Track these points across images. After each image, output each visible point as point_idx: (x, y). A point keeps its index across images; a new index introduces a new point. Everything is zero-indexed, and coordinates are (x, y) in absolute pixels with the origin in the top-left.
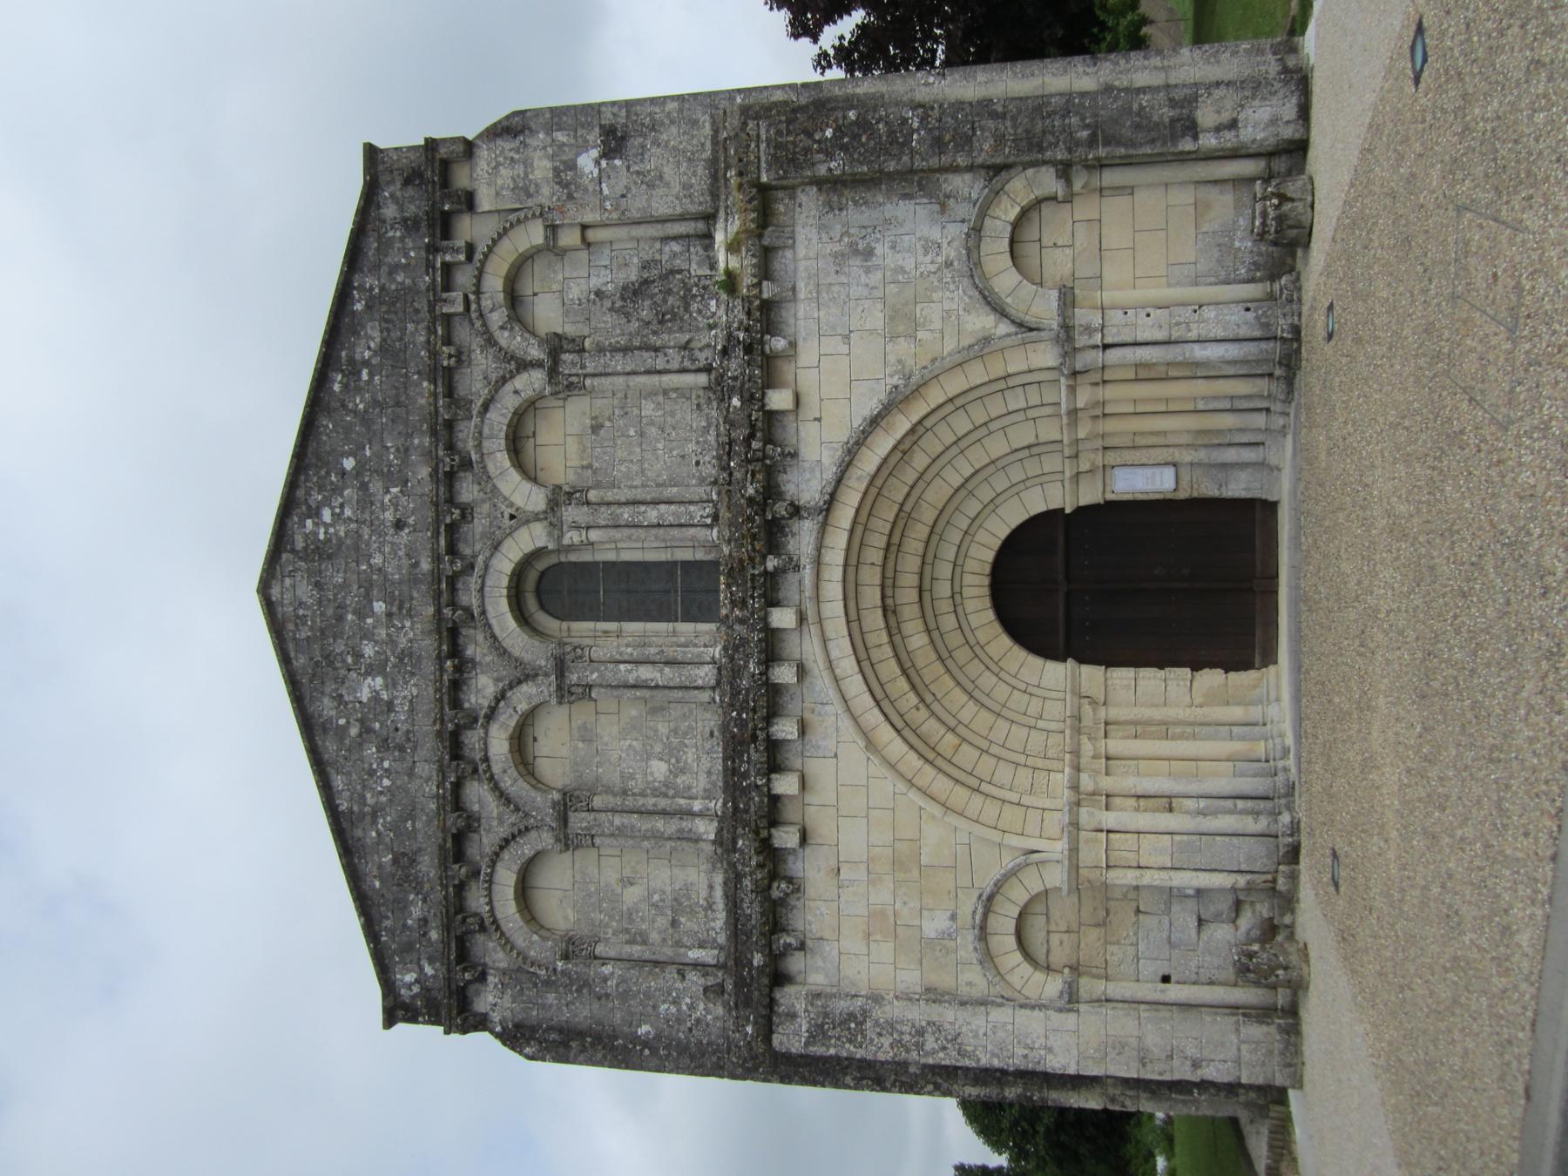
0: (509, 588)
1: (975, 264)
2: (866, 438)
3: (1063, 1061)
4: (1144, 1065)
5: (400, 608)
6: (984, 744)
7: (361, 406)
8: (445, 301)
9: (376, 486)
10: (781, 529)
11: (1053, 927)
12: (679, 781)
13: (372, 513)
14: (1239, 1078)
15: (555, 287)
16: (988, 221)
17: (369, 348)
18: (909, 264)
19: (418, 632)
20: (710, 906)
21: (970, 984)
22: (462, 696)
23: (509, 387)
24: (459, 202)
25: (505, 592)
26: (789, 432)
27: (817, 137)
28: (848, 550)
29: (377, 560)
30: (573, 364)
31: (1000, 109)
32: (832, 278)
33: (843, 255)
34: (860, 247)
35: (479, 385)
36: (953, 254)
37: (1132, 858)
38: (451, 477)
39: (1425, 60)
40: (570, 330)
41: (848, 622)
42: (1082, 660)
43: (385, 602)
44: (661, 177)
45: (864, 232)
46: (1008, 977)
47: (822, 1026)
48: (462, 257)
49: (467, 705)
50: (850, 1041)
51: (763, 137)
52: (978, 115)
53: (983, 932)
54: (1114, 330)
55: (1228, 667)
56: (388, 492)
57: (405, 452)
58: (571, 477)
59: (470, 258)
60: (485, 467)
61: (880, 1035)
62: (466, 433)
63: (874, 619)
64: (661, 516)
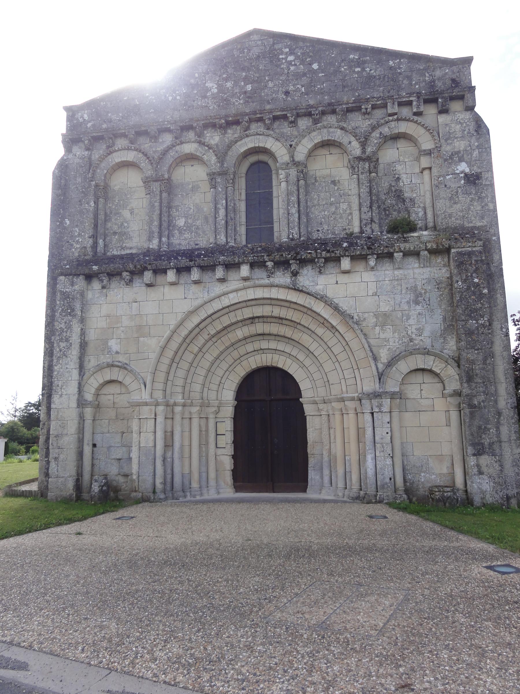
0: (259, 147)
1: (411, 352)
2: (328, 305)
3: (56, 402)
4: (55, 437)
5: (249, 97)
6: (195, 365)
7: (343, 69)
8: (393, 104)
9: (305, 80)
10: (286, 269)
11: (116, 396)
12: (176, 231)
13: (292, 80)
14: (51, 477)
15: (401, 158)
16: (432, 358)
17: (371, 70)
18: (411, 322)
19: (238, 107)
20: (123, 248)
21: (89, 361)
22: (210, 129)
23: (353, 139)
24: (443, 106)
25: (257, 145)
26: (331, 268)
27: (474, 275)
28: (278, 300)
29: (270, 84)
30: (364, 168)
31: (488, 362)
32: (404, 286)
33: (416, 291)
34: (420, 298)
35: (353, 125)
36: (416, 342)
37: (144, 429)
38: (310, 114)
39: (504, 573)
40: (381, 167)
41: (246, 301)
42: (237, 408)
43: (251, 90)
44: (455, 203)
45: (427, 300)
46: (92, 377)
47: (69, 298)
48: (415, 110)
49: (205, 132)
50: (62, 310)
51: (474, 249)
52: (485, 352)
53: (111, 366)
54: (380, 418)
55: (235, 473)
56: (302, 86)
57: (322, 92)
58: (311, 173)
59: (415, 114)
60: (314, 131)
61: (66, 323)
62: (331, 119)
63: (248, 313)
64: (293, 215)
